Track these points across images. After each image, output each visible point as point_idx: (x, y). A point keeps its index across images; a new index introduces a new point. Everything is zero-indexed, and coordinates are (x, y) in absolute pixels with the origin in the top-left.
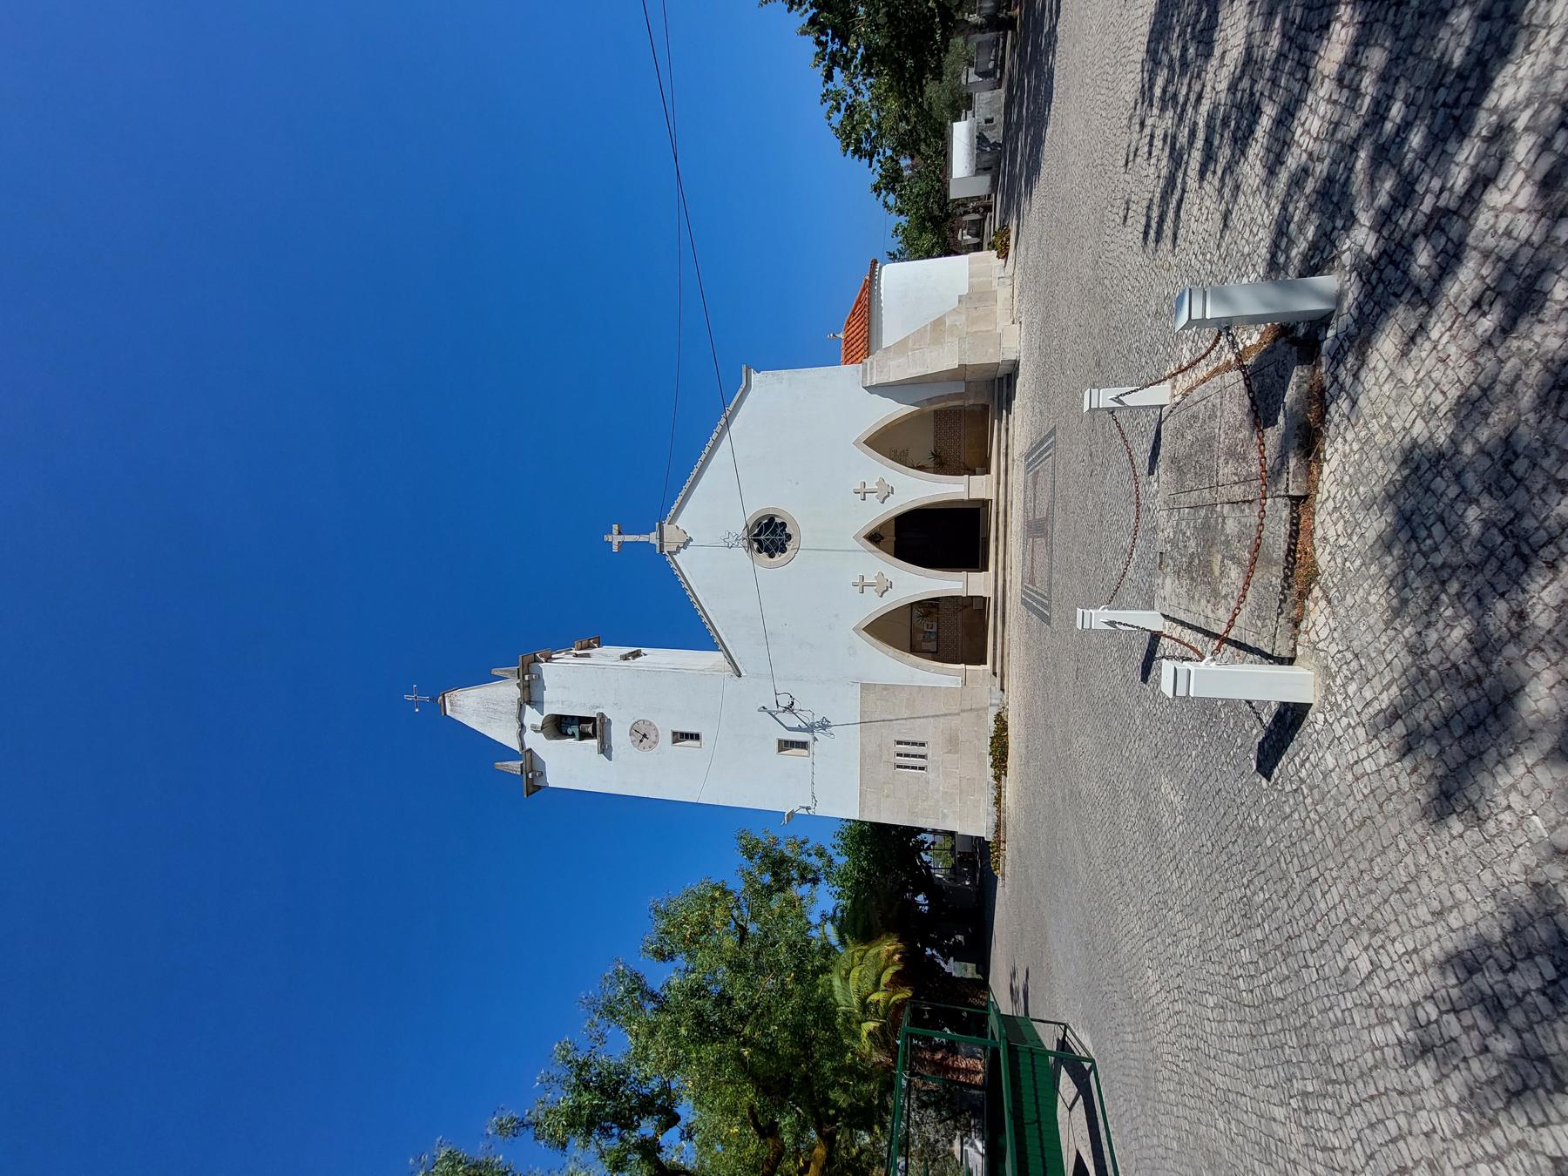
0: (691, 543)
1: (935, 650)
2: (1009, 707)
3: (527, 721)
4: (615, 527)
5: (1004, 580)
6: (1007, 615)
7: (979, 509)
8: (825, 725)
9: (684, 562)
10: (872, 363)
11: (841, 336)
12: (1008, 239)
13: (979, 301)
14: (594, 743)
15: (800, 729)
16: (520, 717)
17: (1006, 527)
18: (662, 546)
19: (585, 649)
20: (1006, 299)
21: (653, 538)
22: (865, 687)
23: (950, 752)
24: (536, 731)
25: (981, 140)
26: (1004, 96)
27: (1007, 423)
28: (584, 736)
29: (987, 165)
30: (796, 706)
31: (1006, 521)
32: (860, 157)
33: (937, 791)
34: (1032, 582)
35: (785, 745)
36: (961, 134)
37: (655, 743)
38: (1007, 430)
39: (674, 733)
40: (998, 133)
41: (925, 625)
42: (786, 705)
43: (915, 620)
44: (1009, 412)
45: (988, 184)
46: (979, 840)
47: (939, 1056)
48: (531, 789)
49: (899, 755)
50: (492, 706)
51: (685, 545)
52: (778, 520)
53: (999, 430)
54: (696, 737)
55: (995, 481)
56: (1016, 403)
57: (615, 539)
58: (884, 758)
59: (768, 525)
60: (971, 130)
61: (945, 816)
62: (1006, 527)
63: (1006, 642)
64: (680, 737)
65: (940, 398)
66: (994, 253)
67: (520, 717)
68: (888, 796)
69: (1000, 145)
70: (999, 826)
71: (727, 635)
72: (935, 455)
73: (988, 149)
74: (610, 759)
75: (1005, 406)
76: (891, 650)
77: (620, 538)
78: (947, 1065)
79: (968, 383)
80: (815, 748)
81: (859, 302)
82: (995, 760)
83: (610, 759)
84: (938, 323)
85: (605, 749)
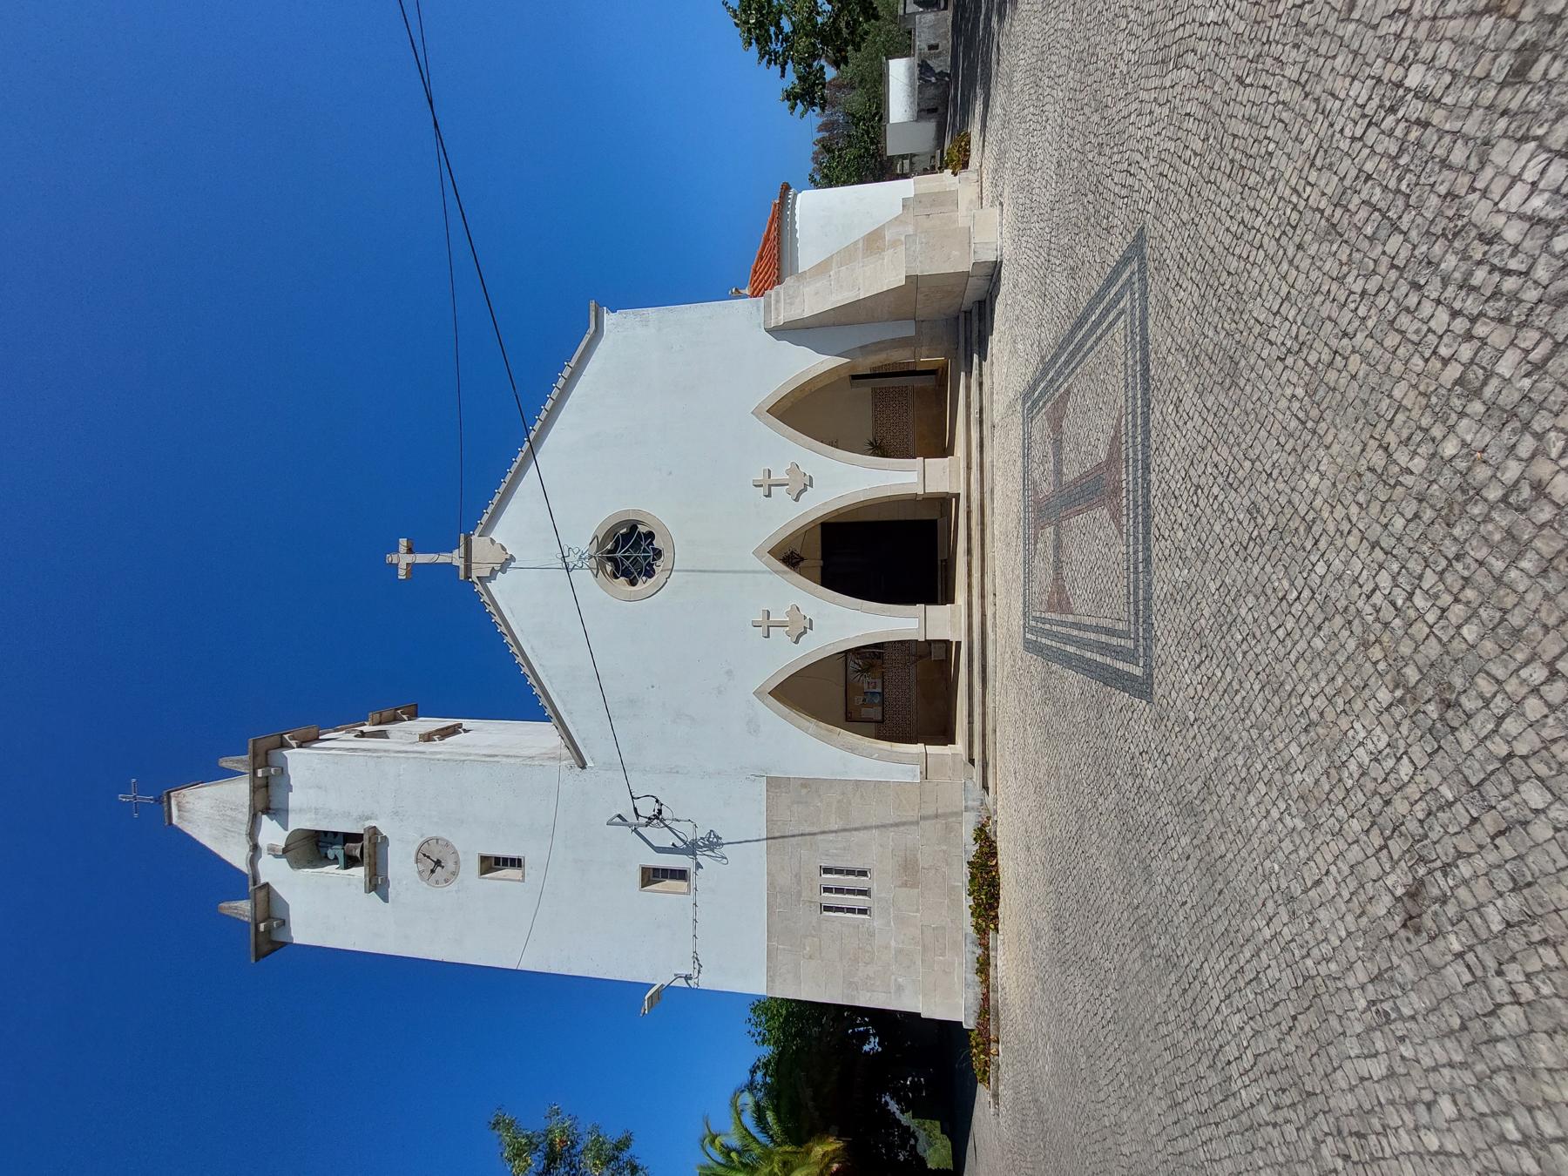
0: (513, 565)
1: (880, 718)
2: (1001, 817)
3: (264, 840)
4: (403, 542)
5: (984, 615)
6: (990, 669)
7: (935, 522)
8: (713, 843)
9: (501, 590)
10: (778, 294)
14: (359, 872)
15: (674, 850)
16: (253, 834)
17: (983, 531)
18: (468, 569)
19: (380, 723)
20: (971, 201)
21: (456, 558)
22: (774, 784)
23: (905, 885)
24: (276, 856)
25: (924, 68)
26: (950, 19)
27: (981, 375)
28: (351, 862)
30: (664, 815)
31: (983, 523)
32: (769, 62)
33: (887, 947)
34: (1060, 602)
35: (652, 876)
36: (899, 71)
37: (454, 874)
38: (981, 384)
39: (484, 859)
40: (945, 61)
41: (867, 683)
42: (650, 814)
43: (851, 677)
44: (983, 357)
45: (935, 128)
46: (950, 1029)
48: (265, 948)
49: (827, 890)
50: (229, 813)
51: (504, 566)
53: (968, 388)
54: (516, 863)
55: (963, 464)
56: (996, 343)
57: (403, 560)
59: (626, 537)
60: (910, 69)
61: (900, 988)
62: (983, 531)
63: (990, 711)
64: (491, 864)
65: (880, 346)
66: (948, 172)
67: (253, 834)
69: (947, 75)
70: (986, 1009)
71: (565, 705)
73: (933, 80)
74: (385, 899)
75: (976, 348)
76: (812, 724)
77: (410, 558)
79: (919, 323)
80: (699, 879)
81: (767, 239)
82: (978, 905)
83: (385, 899)
85: (377, 884)
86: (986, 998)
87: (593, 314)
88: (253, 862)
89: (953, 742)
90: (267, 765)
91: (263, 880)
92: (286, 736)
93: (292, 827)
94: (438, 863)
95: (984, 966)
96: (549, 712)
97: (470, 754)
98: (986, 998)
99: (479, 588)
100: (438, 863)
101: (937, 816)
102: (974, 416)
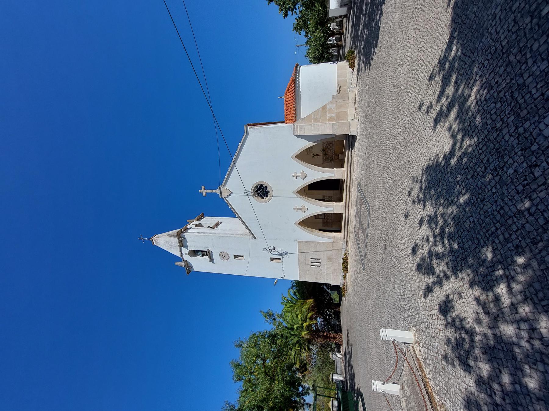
4: (203, 187)
5: (349, 211)
6: (349, 223)
8: (286, 253)
11: (284, 97)
12: (354, 62)
13: (341, 98)
15: (277, 255)
16: (180, 251)
17: (350, 192)
18: (221, 195)
21: (217, 191)
27: (352, 153)
28: (203, 255)
29: (346, 4)
31: (350, 190)
33: (325, 273)
35: (272, 259)
44: (352, 149)
47: (325, 334)
48: (189, 272)
51: (230, 195)
52: (264, 186)
53: (348, 154)
58: (307, 263)
61: (327, 280)
62: (350, 192)
64: (236, 257)
68: (308, 274)
70: (344, 285)
72: (323, 151)
75: (350, 146)
77: (205, 191)
78: (328, 336)
84: (324, 108)
85: (211, 260)
86: (345, 283)
87: (245, 129)
88: (182, 256)
89: (342, 202)
90: (181, 237)
91: (185, 260)
92: (182, 230)
93: (189, 250)
94: (225, 256)
95: (344, 278)
96: (237, 216)
97: (227, 234)
98: (345, 283)
99: (225, 200)
100: (225, 256)
101: (336, 249)
102: (349, 164)
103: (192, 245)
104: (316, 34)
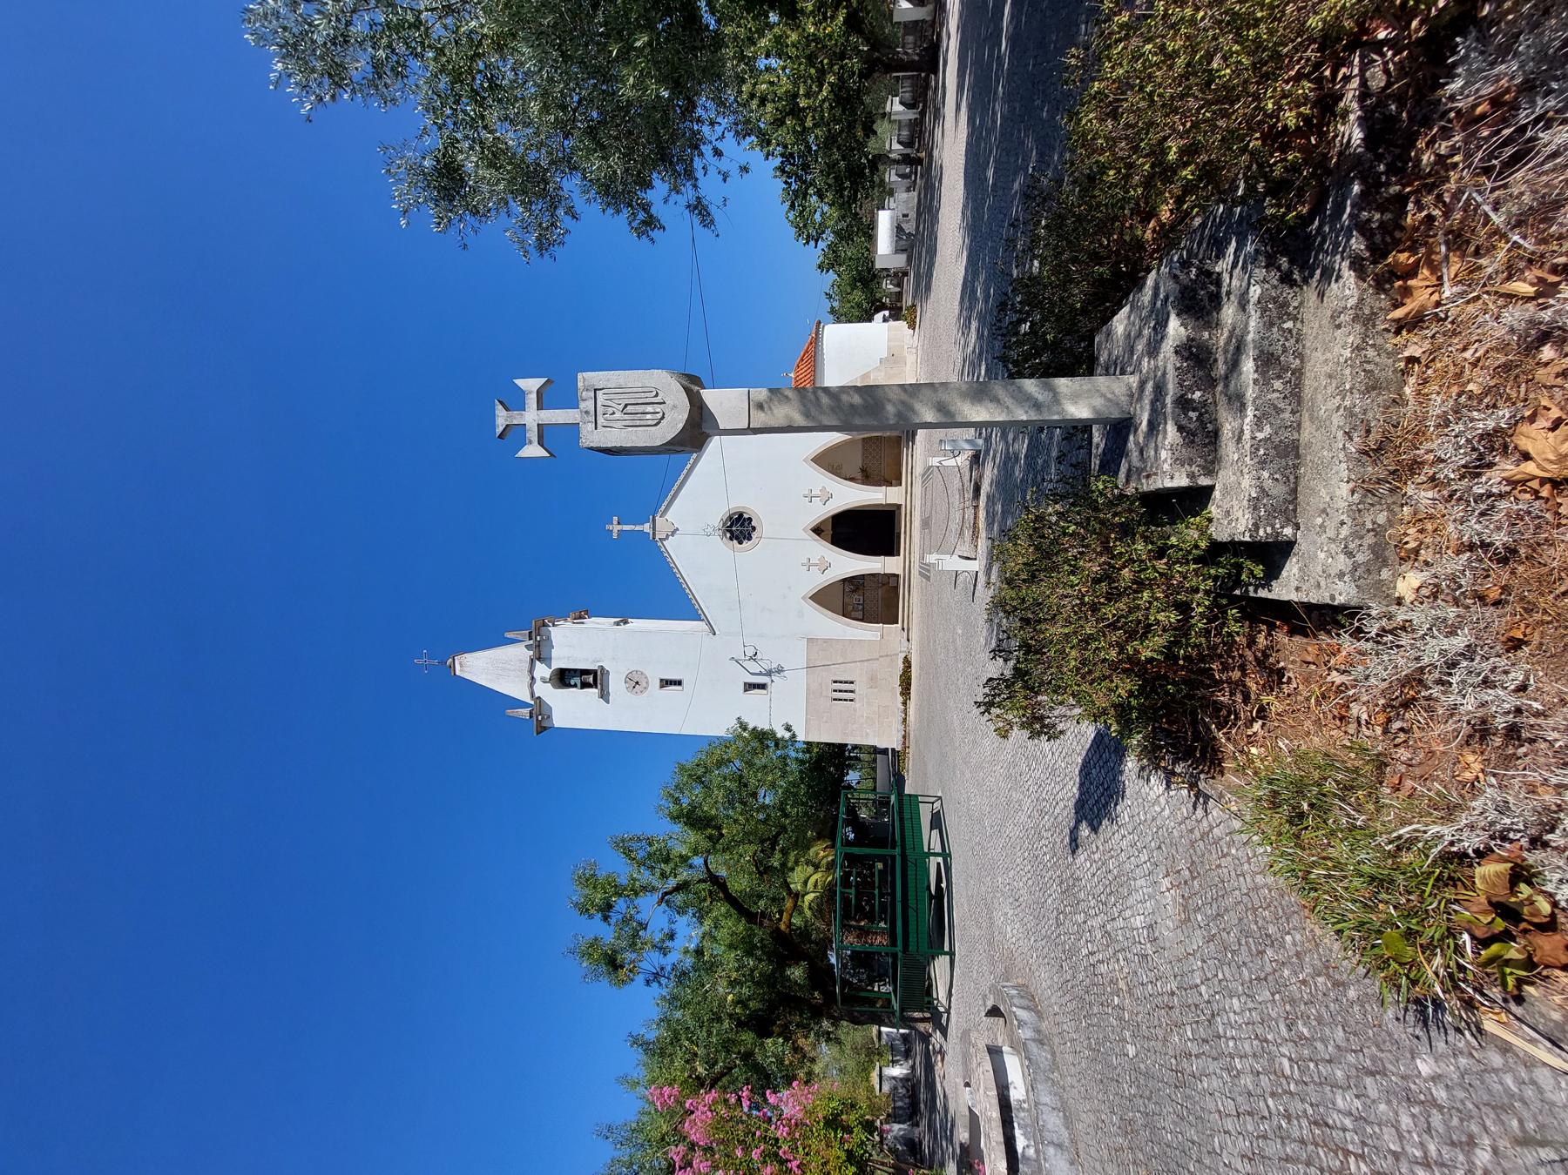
8: (780, 670)
21: (647, 528)
44: (913, 443)
51: (673, 533)
52: (745, 516)
58: (824, 694)
64: (666, 683)
72: (863, 470)
77: (620, 527)
94: (637, 683)
100: (637, 683)
103: (563, 657)
104: (852, 297)
